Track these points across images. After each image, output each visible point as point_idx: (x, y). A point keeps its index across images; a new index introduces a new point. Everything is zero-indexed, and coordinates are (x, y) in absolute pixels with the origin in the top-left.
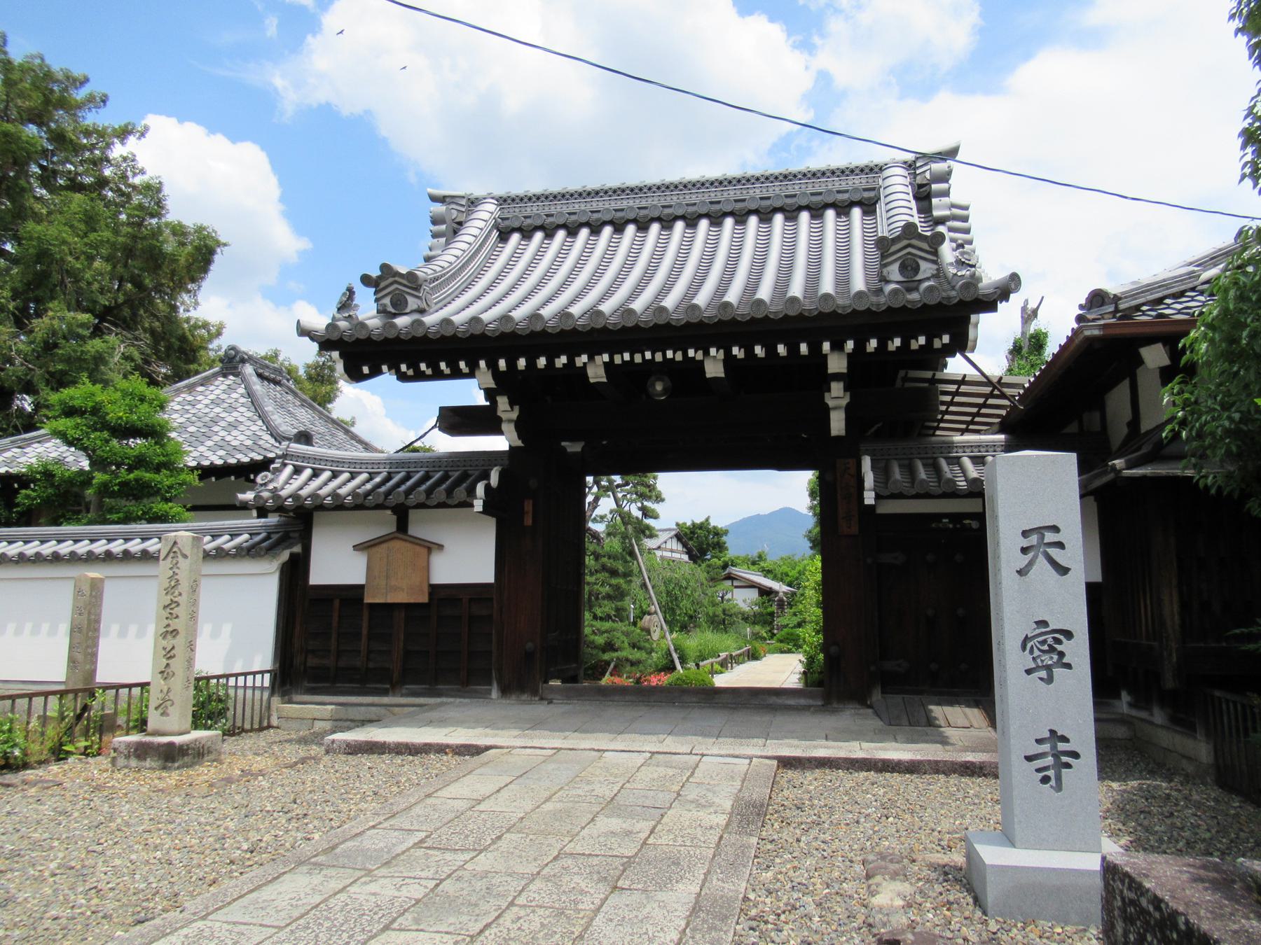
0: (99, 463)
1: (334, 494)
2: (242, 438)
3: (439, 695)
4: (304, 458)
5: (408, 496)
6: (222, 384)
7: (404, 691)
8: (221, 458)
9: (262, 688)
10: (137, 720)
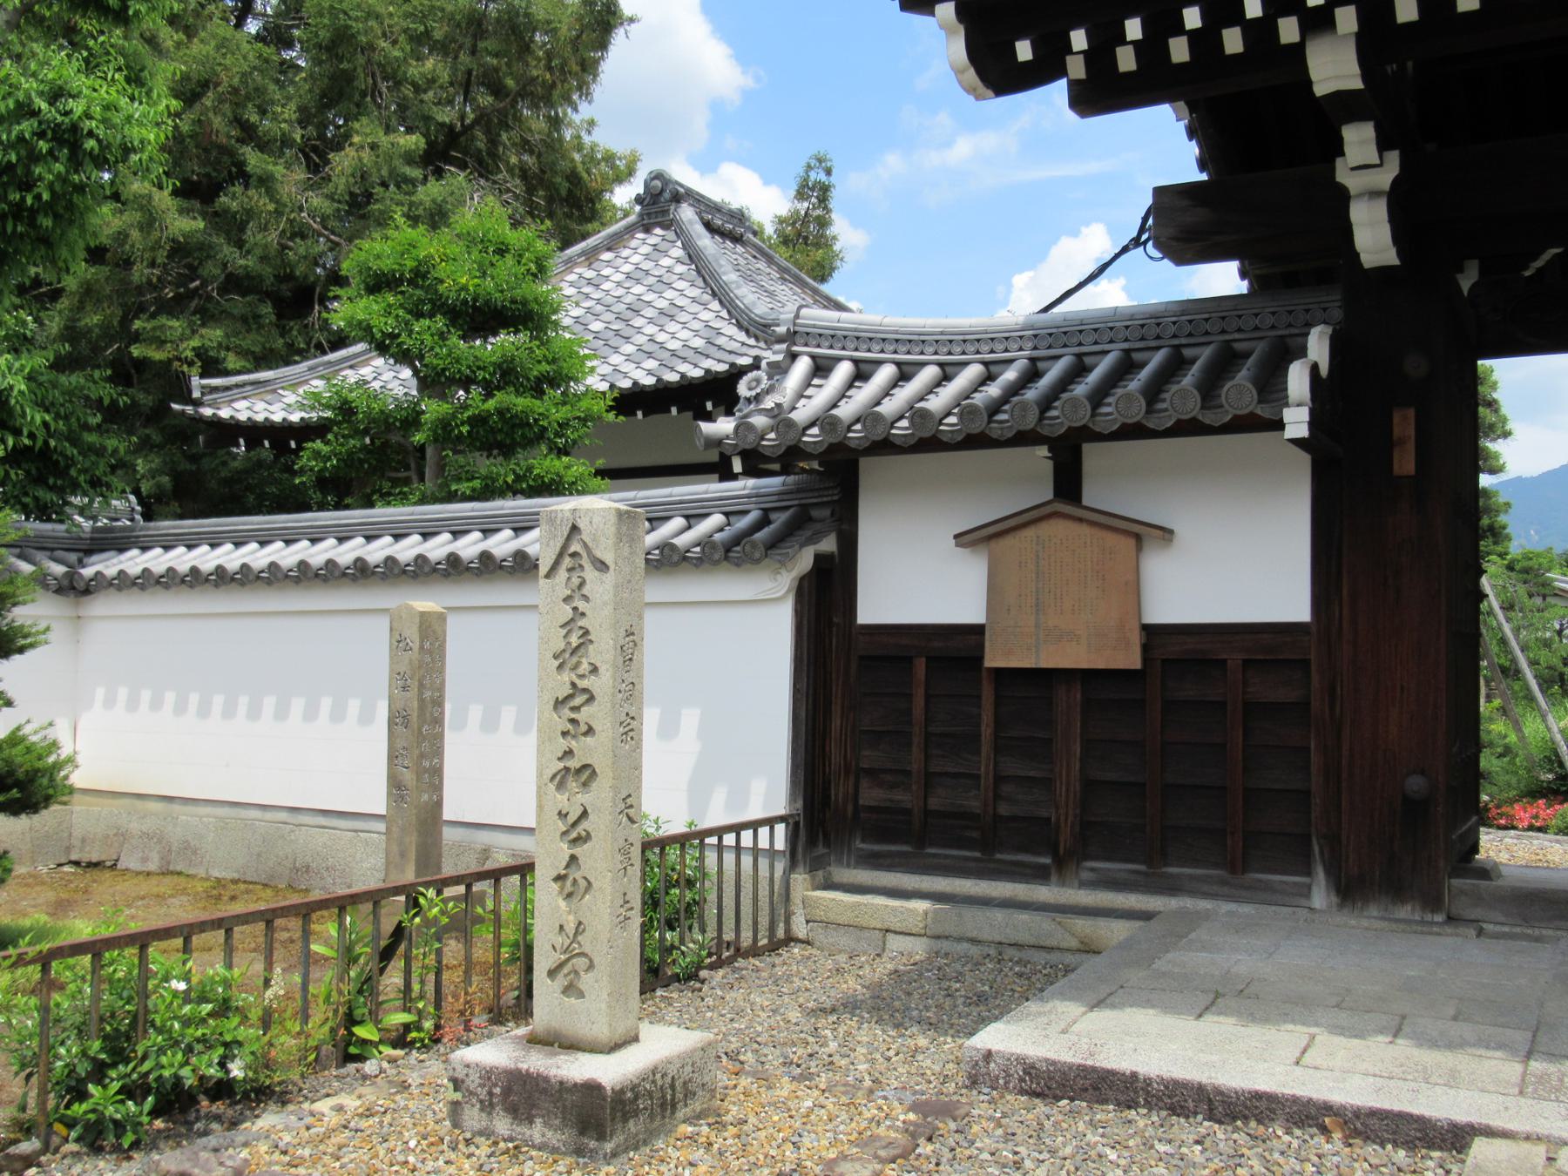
0: (432, 383)
1: (917, 414)
2: (684, 334)
3: (1172, 888)
4: (834, 337)
5: (1067, 419)
6: (642, 244)
7: (1085, 875)
8: (650, 373)
9: (772, 853)
10: (516, 945)
